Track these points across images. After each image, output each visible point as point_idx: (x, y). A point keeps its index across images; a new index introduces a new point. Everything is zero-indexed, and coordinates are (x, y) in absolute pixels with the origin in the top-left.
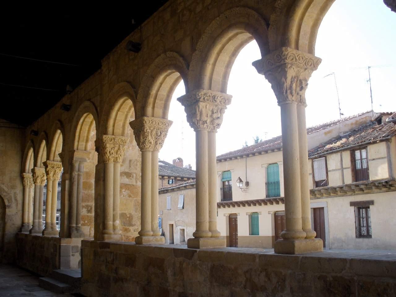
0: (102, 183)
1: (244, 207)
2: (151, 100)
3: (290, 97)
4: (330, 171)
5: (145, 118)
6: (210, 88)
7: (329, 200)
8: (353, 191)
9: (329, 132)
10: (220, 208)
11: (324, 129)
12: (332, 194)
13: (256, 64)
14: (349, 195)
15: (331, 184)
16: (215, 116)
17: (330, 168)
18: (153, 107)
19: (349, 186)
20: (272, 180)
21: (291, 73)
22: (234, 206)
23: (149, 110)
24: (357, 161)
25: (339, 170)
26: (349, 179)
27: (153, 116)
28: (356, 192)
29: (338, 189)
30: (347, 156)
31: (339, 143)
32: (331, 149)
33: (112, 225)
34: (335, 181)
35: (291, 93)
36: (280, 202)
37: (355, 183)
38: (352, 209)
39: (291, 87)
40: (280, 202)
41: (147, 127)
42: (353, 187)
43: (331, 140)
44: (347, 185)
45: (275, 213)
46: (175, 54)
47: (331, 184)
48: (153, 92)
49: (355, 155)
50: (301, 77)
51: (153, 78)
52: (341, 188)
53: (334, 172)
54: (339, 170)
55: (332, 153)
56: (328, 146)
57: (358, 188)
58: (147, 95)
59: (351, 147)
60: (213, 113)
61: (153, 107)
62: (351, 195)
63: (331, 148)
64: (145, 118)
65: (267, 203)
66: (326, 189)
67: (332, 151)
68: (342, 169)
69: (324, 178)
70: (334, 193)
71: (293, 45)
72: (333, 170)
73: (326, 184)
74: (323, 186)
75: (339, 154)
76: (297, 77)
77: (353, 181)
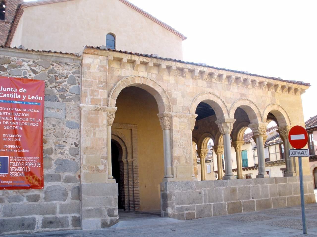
0: (262, 177)
1: (247, 171)
2: (203, 144)
3: (238, 150)
4: (271, 154)
5: (202, 149)
6: (220, 145)
7: (271, 168)
8: (282, 163)
9: (272, 133)
10: (248, 170)
11: (269, 132)
12: (272, 165)
13: (196, 150)
14: (280, 165)
15: (271, 160)
16: (221, 151)
17: (271, 152)
18: (203, 146)
19: (279, 161)
20: (244, 158)
21: (238, 145)
22: (250, 169)
23: (202, 147)
24: (282, 149)
25: (274, 153)
26: (279, 158)
27: (203, 149)
28: (283, 164)
29: (274, 162)
30: (278, 146)
31: (274, 141)
32: (271, 143)
33: (288, 161)
34: (273, 159)
35: (238, 149)
36: (248, 169)
37: (282, 159)
38: (282, 171)
39: (238, 148)
40: (248, 169)
41: (202, 152)
42: (281, 162)
43: (273, 137)
44: (278, 161)
45: (246, 175)
46: (210, 134)
47: (271, 160)
48: (203, 142)
49: (281, 147)
50: (240, 146)
51: (203, 138)
52: (276, 162)
53: (272, 154)
54: (274, 153)
55: (271, 145)
56: (270, 142)
57: (283, 162)
58: (201, 143)
59: (279, 143)
60: (221, 150)
61: (203, 146)
62: (281, 165)
63: (271, 143)
64: (202, 149)
65: (248, 169)
66: (270, 163)
67: (271, 144)
68: (276, 153)
69: (268, 157)
70: (273, 164)
71: (238, 140)
72: (272, 154)
73: (269, 160)
74: (268, 161)
75: (274, 146)
76: (239, 146)
77: (281, 159)
